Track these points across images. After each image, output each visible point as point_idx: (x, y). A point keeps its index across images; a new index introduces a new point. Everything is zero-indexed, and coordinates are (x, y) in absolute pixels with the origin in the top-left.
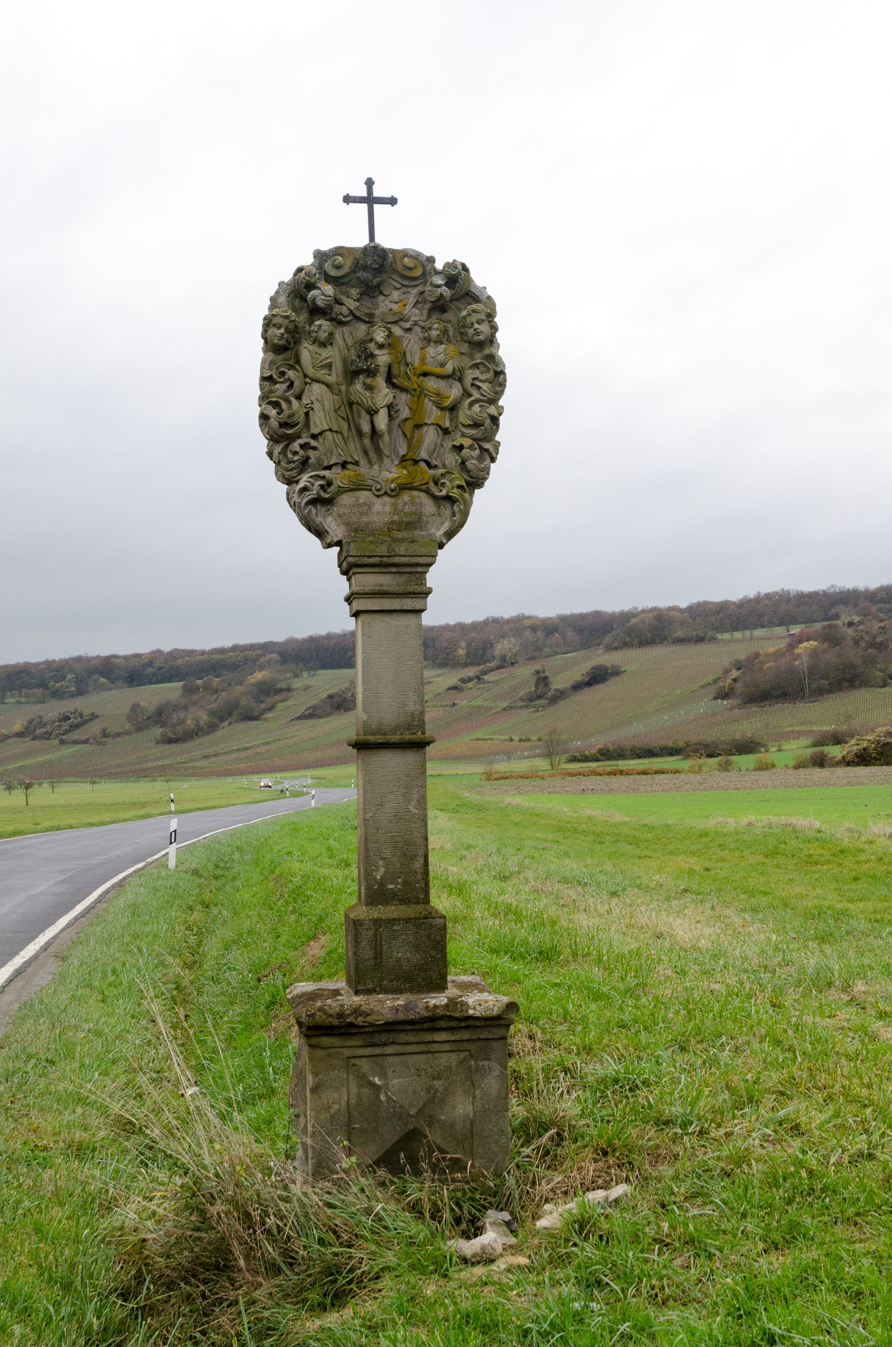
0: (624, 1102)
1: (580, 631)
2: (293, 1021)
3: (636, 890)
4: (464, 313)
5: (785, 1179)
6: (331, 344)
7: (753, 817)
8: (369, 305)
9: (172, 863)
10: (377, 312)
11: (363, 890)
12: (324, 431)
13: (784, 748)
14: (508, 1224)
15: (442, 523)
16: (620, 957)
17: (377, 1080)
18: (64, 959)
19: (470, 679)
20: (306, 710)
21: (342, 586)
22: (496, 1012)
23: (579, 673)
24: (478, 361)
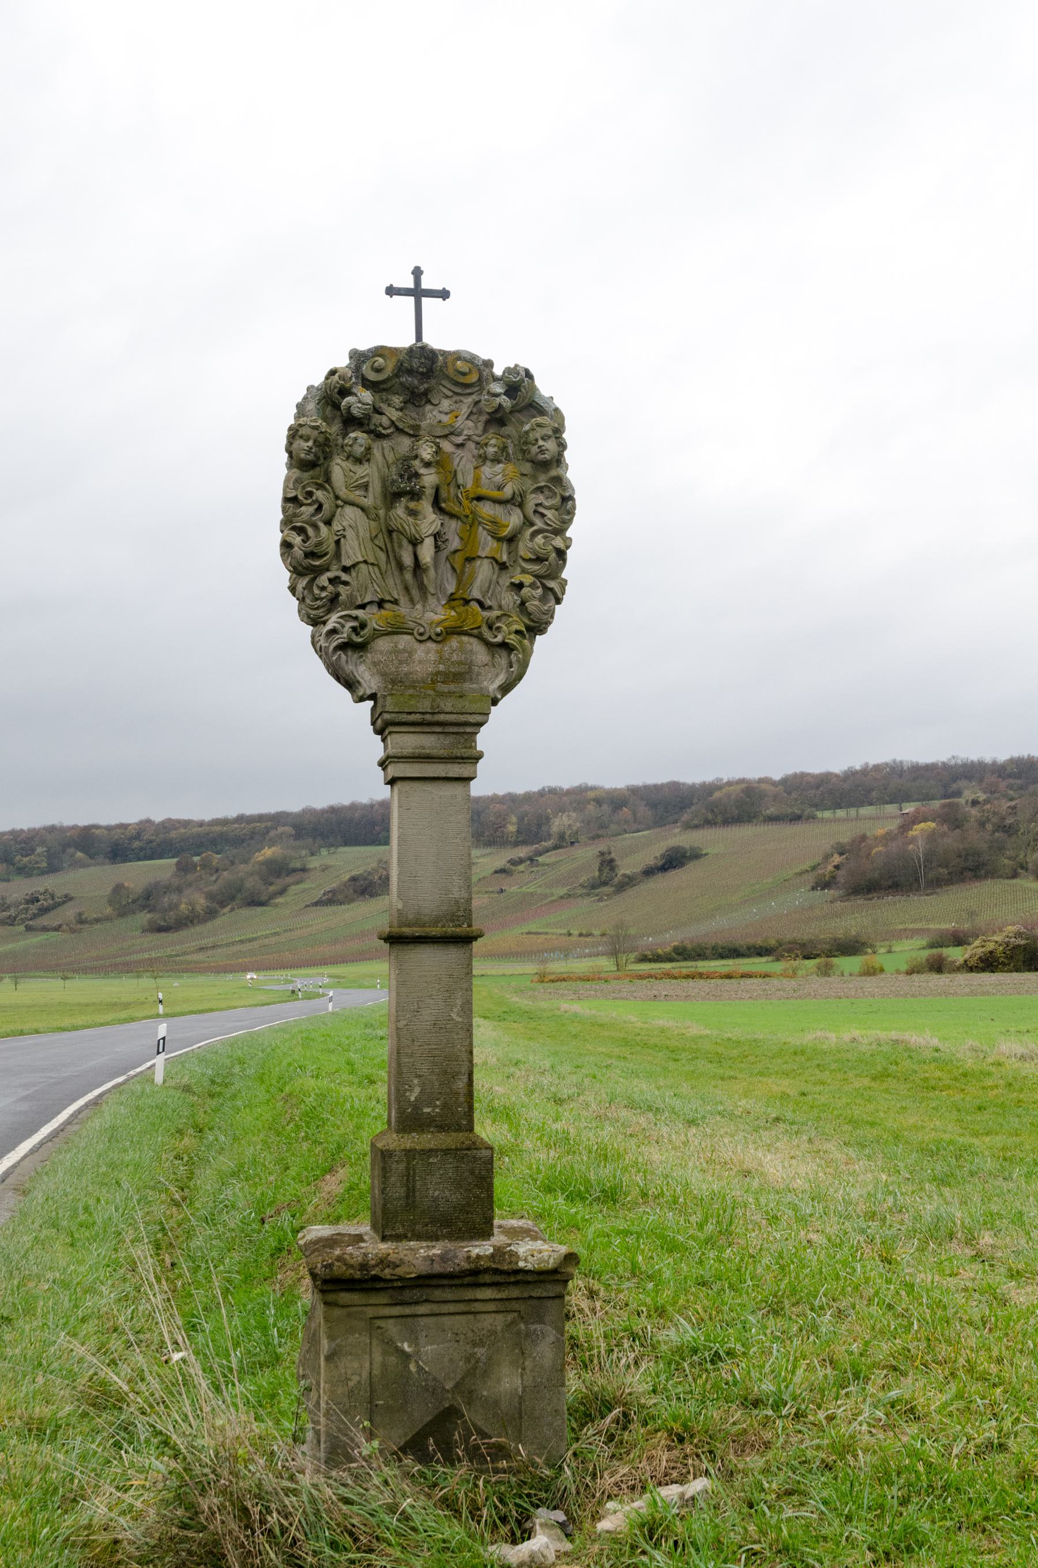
0: (704, 1376)
1: (653, 805)
2: (304, 1271)
3: (718, 1118)
4: (527, 427)
5: (899, 1474)
6: (368, 460)
7: (858, 1032)
8: (414, 415)
9: (159, 1077)
10: (424, 424)
11: (393, 1114)
12: (358, 563)
13: (894, 949)
14: (562, 1525)
15: (497, 676)
16: (699, 1201)
17: (406, 1347)
18: (25, 1193)
19: (521, 861)
20: (324, 894)
21: (376, 748)
22: (551, 1264)
23: (652, 855)
24: (543, 484)
